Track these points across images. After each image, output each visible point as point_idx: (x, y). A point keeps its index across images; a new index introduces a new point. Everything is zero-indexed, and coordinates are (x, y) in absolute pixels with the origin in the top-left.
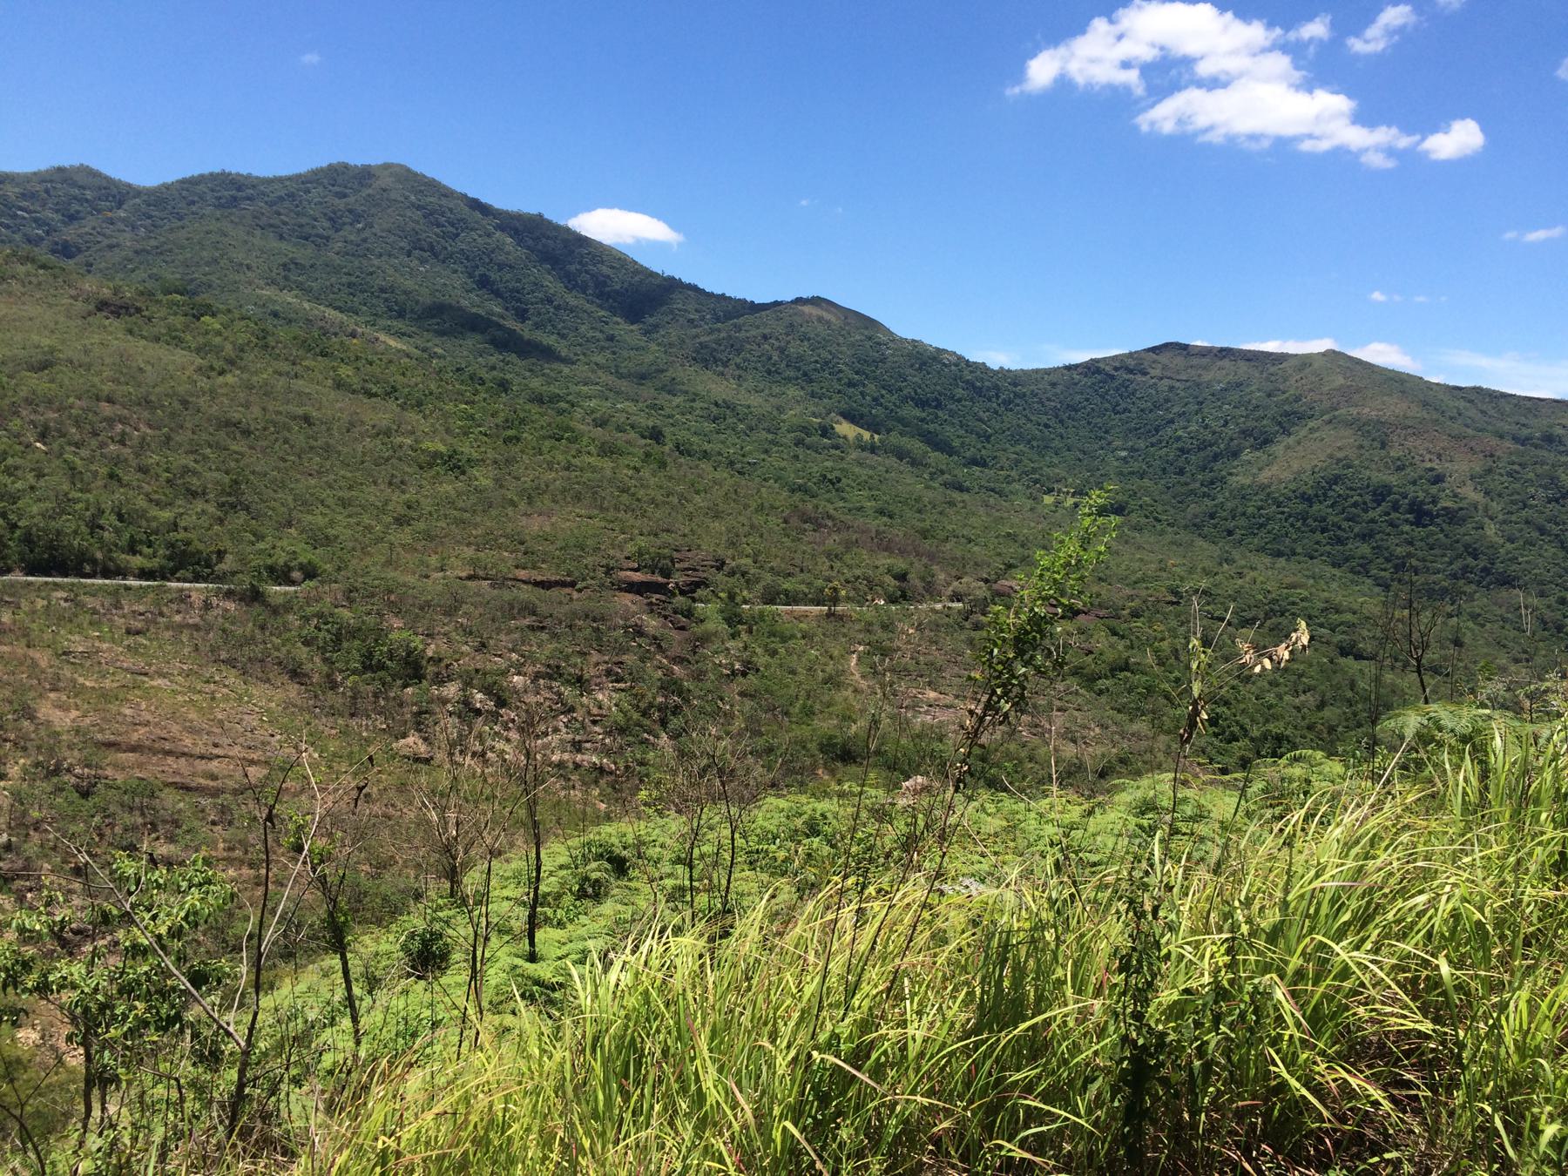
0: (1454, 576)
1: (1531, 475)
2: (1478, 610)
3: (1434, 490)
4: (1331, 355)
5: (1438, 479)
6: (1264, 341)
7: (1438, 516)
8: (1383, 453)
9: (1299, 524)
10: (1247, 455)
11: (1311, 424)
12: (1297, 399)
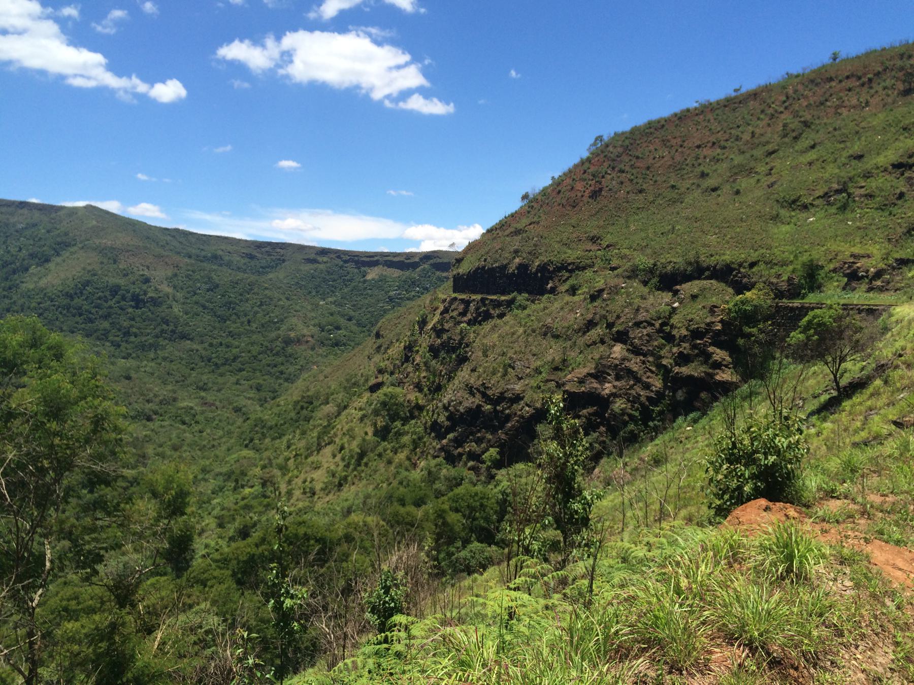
0: (157, 336)
1: (198, 277)
2: (167, 355)
3: (145, 287)
4: (90, 209)
5: (147, 281)
6: (104, 199)
7: (148, 302)
8: (115, 266)
9: (65, 312)
10: (33, 270)
11: (72, 249)
12: (66, 234)
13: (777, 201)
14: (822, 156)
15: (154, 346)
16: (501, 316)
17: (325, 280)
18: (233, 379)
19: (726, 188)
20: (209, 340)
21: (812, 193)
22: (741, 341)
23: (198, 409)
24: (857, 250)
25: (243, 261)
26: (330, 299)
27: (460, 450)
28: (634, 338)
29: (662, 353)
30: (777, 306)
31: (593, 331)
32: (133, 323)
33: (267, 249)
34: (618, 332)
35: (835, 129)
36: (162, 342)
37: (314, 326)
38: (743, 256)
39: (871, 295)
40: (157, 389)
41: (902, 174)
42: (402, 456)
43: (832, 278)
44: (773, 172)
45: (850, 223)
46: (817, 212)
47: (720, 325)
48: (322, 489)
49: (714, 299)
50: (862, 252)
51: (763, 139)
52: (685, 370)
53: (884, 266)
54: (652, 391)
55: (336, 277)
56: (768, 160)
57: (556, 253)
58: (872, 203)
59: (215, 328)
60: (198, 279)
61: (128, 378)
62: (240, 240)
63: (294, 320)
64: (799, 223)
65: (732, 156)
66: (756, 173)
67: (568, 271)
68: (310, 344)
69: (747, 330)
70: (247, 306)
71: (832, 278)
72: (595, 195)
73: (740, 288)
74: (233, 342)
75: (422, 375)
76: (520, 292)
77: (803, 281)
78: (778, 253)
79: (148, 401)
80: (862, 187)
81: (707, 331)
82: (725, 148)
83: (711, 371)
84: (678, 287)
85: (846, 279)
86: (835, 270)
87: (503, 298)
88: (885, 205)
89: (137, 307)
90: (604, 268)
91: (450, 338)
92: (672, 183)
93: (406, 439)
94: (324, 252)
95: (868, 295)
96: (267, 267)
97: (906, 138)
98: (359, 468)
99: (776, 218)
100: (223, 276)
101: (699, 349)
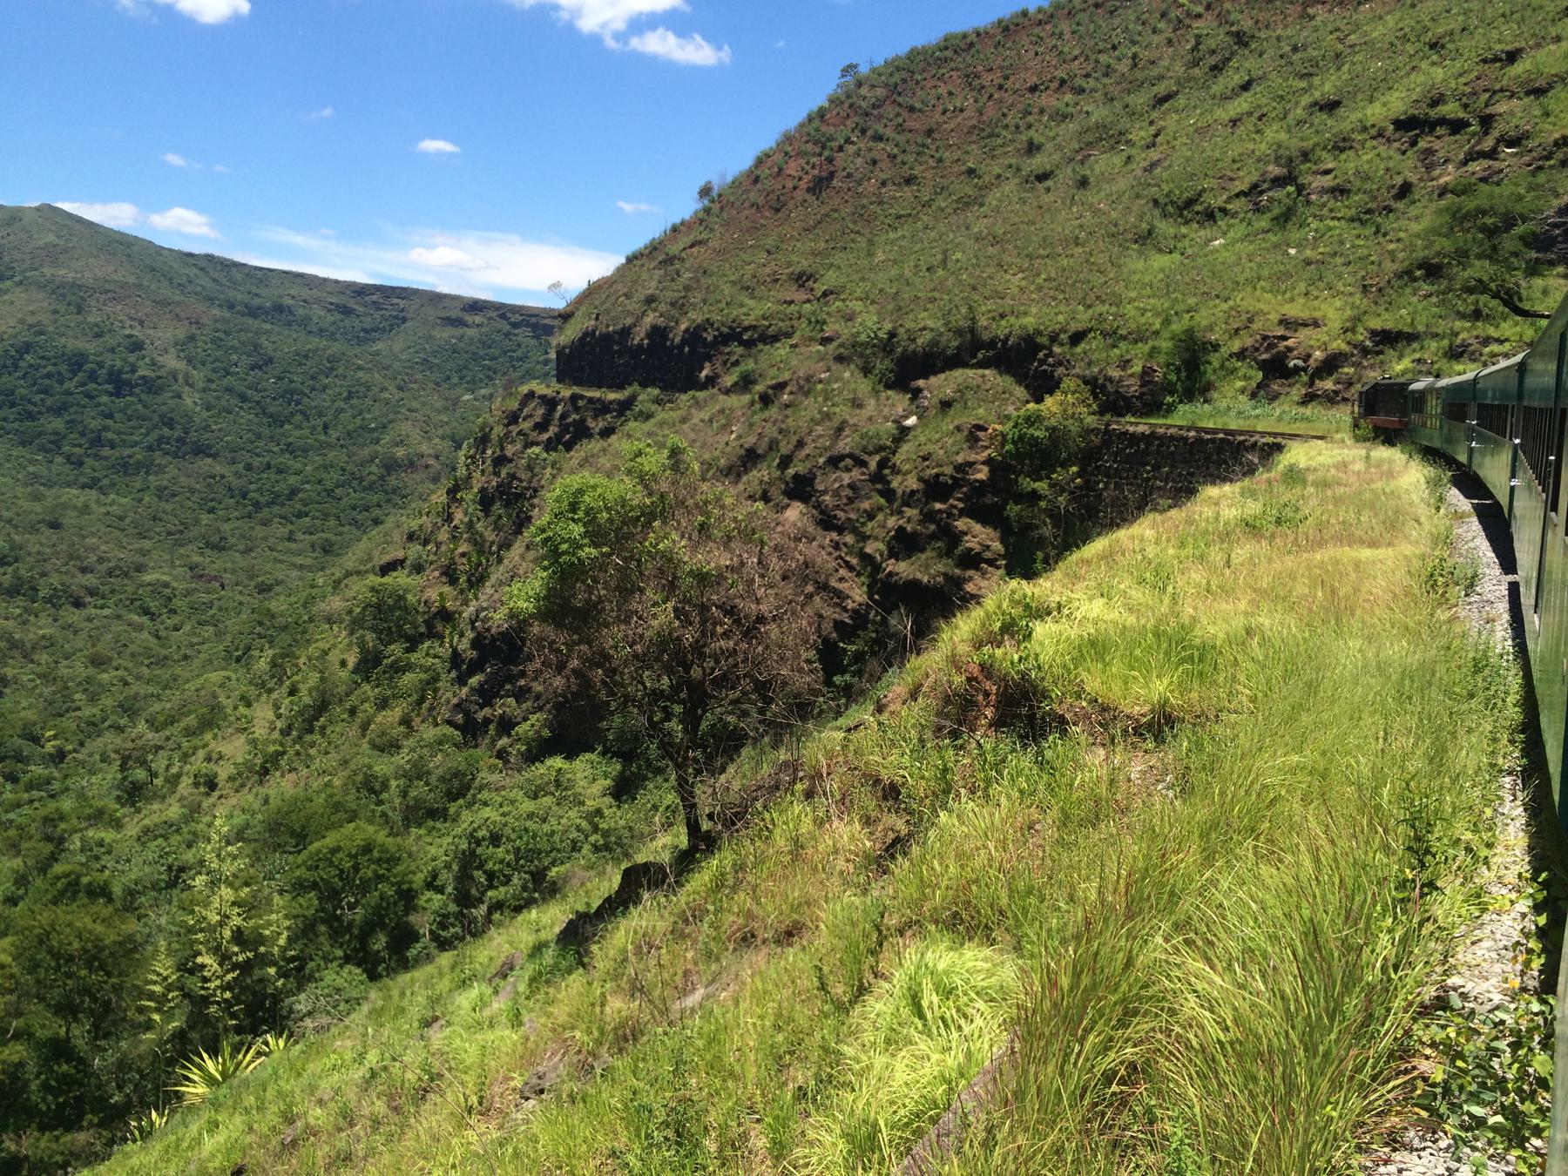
0: (150, 448)
2: (165, 483)
3: (132, 358)
5: (137, 346)
7: (137, 385)
13: (1156, 202)
14: (1259, 106)
15: (146, 467)
16: (607, 433)
17: (475, 358)
18: (283, 531)
19: (1066, 175)
20: (247, 458)
21: (1228, 185)
22: (1013, 510)
23: (180, 586)
24: (1295, 310)
25: (330, 318)
26: (483, 391)
27: (487, 711)
28: (825, 492)
29: (869, 528)
30: (1107, 431)
31: (755, 472)
32: (109, 422)
33: (374, 298)
34: (796, 476)
35: (1295, 49)
36: (159, 458)
37: (443, 438)
38: (1061, 318)
39: (1308, 411)
40: (103, 547)
41: (1414, 143)
42: (393, 715)
43: (1234, 371)
44: (1159, 139)
45: (1292, 251)
46: (1230, 226)
47: (986, 469)
48: (231, 779)
49: (981, 411)
50: (1305, 315)
51: (1155, 72)
52: (903, 569)
53: (1344, 347)
54: (845, 609)
55: (495, 351)
56: (1154, 115)
57: (723, 305)
58: (1344, 208)
59: (259, 436)
60: (232, 347)
61: (55, 526)
62: (325, 280)
63: (405, 428)
64: (1189, 251)
65: (1089, 108)
66: (1128, 142)
67: (742, 343)
68: (432, 470)
69: (1027, 484)
70: (322, 400)
71: (1234, 371)
72: (819, 185)
73: (1042, 386)
74: (290, 463)
75: (461, 550)
76: (644, 385)
77: (1173, 377)
78: (1133, 313)
79: (84, 570)
80: (1327, 172)
81: (957, 483)
82: (1081, 91)
83: (957, 571)
84: (921, 383)
85: (1260, 375)
86: (1241, 355)
87: (612, 396)
88: (1369, 212)
89: (118, 394)
90: (811, 339)
91: (513, 476)
92: (970, 164)
93: (408, 679)
94: (476, 306)
95: (1301, 410)
96: (373, 330)
97: (1434, 64)
98: (308, 738)
99: (1146, 238)
100: (282, 342)
101: (938, 524)
